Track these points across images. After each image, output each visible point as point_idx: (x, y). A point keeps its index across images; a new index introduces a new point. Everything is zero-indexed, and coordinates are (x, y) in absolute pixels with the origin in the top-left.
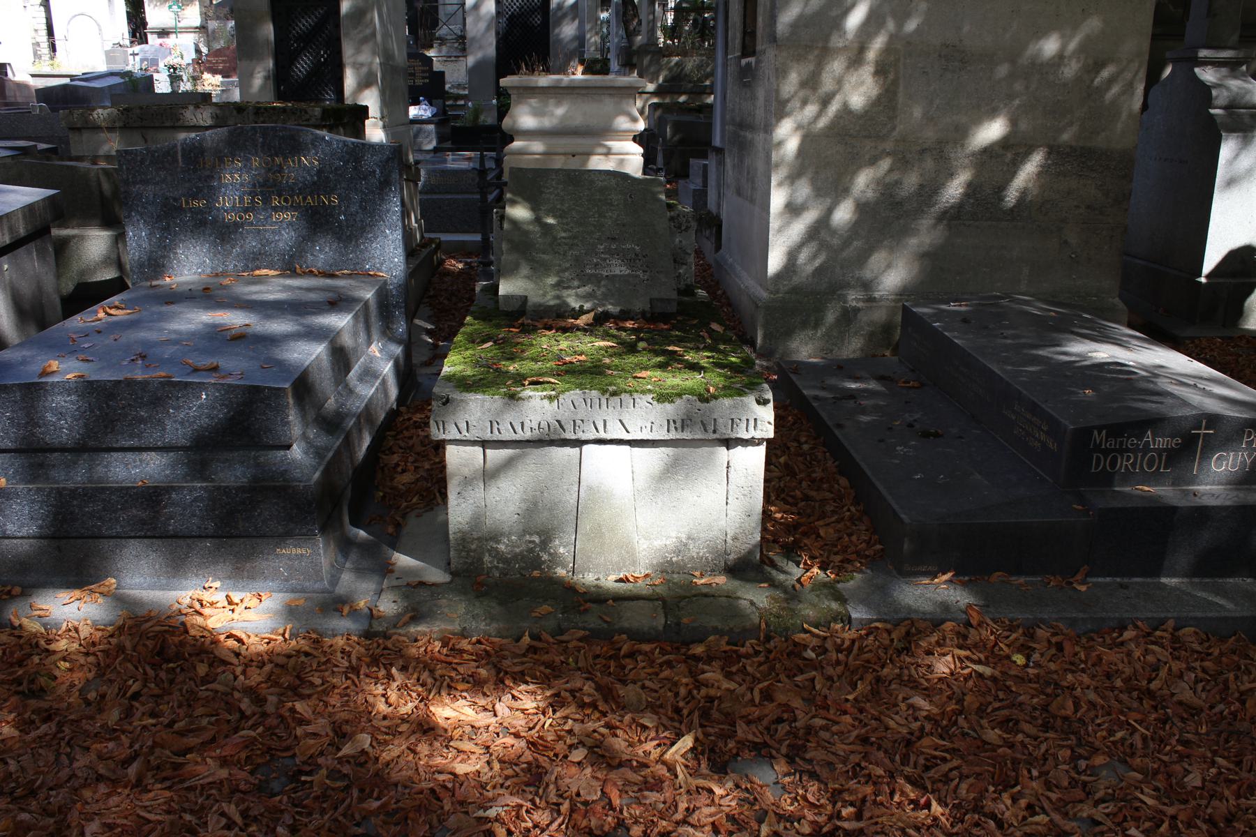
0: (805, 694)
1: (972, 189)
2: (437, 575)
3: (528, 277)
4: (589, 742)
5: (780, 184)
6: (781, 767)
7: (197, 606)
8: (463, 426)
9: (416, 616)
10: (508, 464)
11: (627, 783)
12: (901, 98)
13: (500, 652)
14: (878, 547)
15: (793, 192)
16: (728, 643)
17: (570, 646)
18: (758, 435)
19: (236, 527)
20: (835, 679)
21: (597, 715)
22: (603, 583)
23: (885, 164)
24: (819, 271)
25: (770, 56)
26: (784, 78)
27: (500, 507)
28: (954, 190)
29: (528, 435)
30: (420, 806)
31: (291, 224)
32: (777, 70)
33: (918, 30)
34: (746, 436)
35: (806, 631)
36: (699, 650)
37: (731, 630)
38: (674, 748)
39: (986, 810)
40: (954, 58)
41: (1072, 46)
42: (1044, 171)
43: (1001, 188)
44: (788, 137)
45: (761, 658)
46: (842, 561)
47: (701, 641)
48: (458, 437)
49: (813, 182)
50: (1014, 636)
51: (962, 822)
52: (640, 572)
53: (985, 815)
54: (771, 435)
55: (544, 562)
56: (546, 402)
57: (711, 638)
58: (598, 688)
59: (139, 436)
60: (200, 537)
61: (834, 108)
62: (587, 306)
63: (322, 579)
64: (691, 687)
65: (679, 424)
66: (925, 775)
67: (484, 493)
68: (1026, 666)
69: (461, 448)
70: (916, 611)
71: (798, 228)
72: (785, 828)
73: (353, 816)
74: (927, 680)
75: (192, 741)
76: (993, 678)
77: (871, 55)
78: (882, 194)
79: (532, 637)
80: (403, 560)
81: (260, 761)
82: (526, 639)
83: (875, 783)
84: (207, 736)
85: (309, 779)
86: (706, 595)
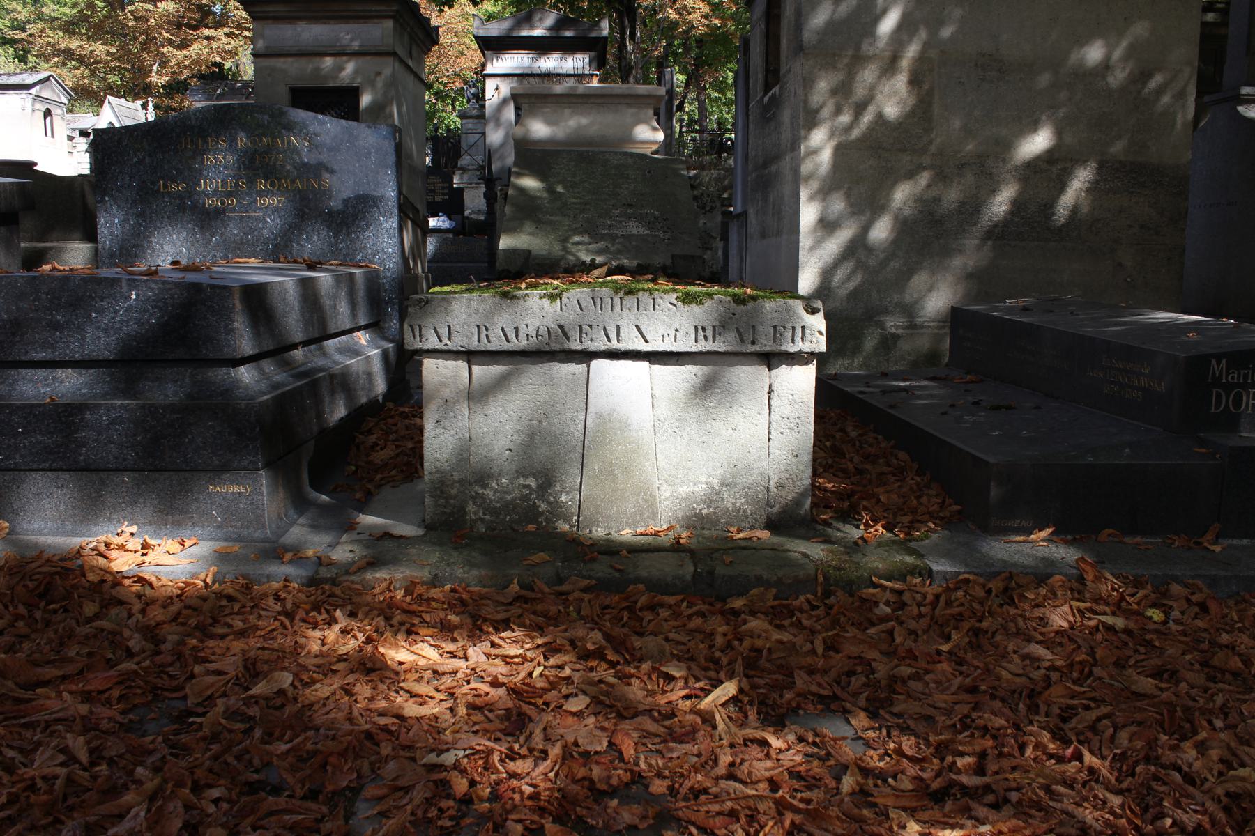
0: (884, 647)
1: (1017, 205)
2: (407, 530)
3: (530, 234)
4: (593, 690)
5: (812, 198)
6: (860, 721)
7: (102, 548)
8: (444, 331)
9: (373, 563)
10: (501, 383)
11: (647, 734)
12: (936, 110)
13: (480, 599)
14: (956, 508)
15: (825, 208)
16: (775, 598)
17: (571, 598)
18: (807, 347)
19: (161, 464)
20: (920, 632)
21: (605, 666)
22: (615, 536)
23: (924, 179)
24: (854, 295)
25: (794, 68)
26: (811, 88)
27: (486, 441)
28: (1001, 203)
29: (523, 344)
30: (346, 749)
31: (277, 210)
32: (804, 79)
33: (953, 38)
34: (792, 349)
35: (875, 586)
36: (738, 603)
37: (780, 581)
38: (710, 698)
39: (1164, 760)
40: (991, 68)
41: (1117, 54)
42: (1092, 188)
43: (1049, 207)
44: (820, 147)
45: (821, 612)
46: (911, 522)
47: (740, 595)
48: (438, 346)
49: (848, 196)
50: (1141, 593)
51: (1133, 775)
52: (661, 526)
53: (1164, 767)
54: (823, 348)
55: (542, 514)
56: (546, 302)
57: (755, 591)
58: (607, 637)
59: (54, 347)
60: (117, 470)
61: (867, 118)
62: (599, 260)
63: (264, 527)
64: (730, 637)
65: (709, 333)
66: (1066, 727)
67: (471, 424)
68: (1165, 623)
69: (441, 363)
70: (1015, 565)
71: (833, 246)
72: (876, 785)
73: (250, 762)
74: (1041, 634)
75: (49, 672)
76: (1127, 631)
77: (905, 63)
78: (920, 212)
79: (522, 586)
80: (368, 520)
81: (137, 701)
82: (515, 587)
83: (994, 737)
84: (69, 669)
85: (199, 720)
86: (745, 548)
